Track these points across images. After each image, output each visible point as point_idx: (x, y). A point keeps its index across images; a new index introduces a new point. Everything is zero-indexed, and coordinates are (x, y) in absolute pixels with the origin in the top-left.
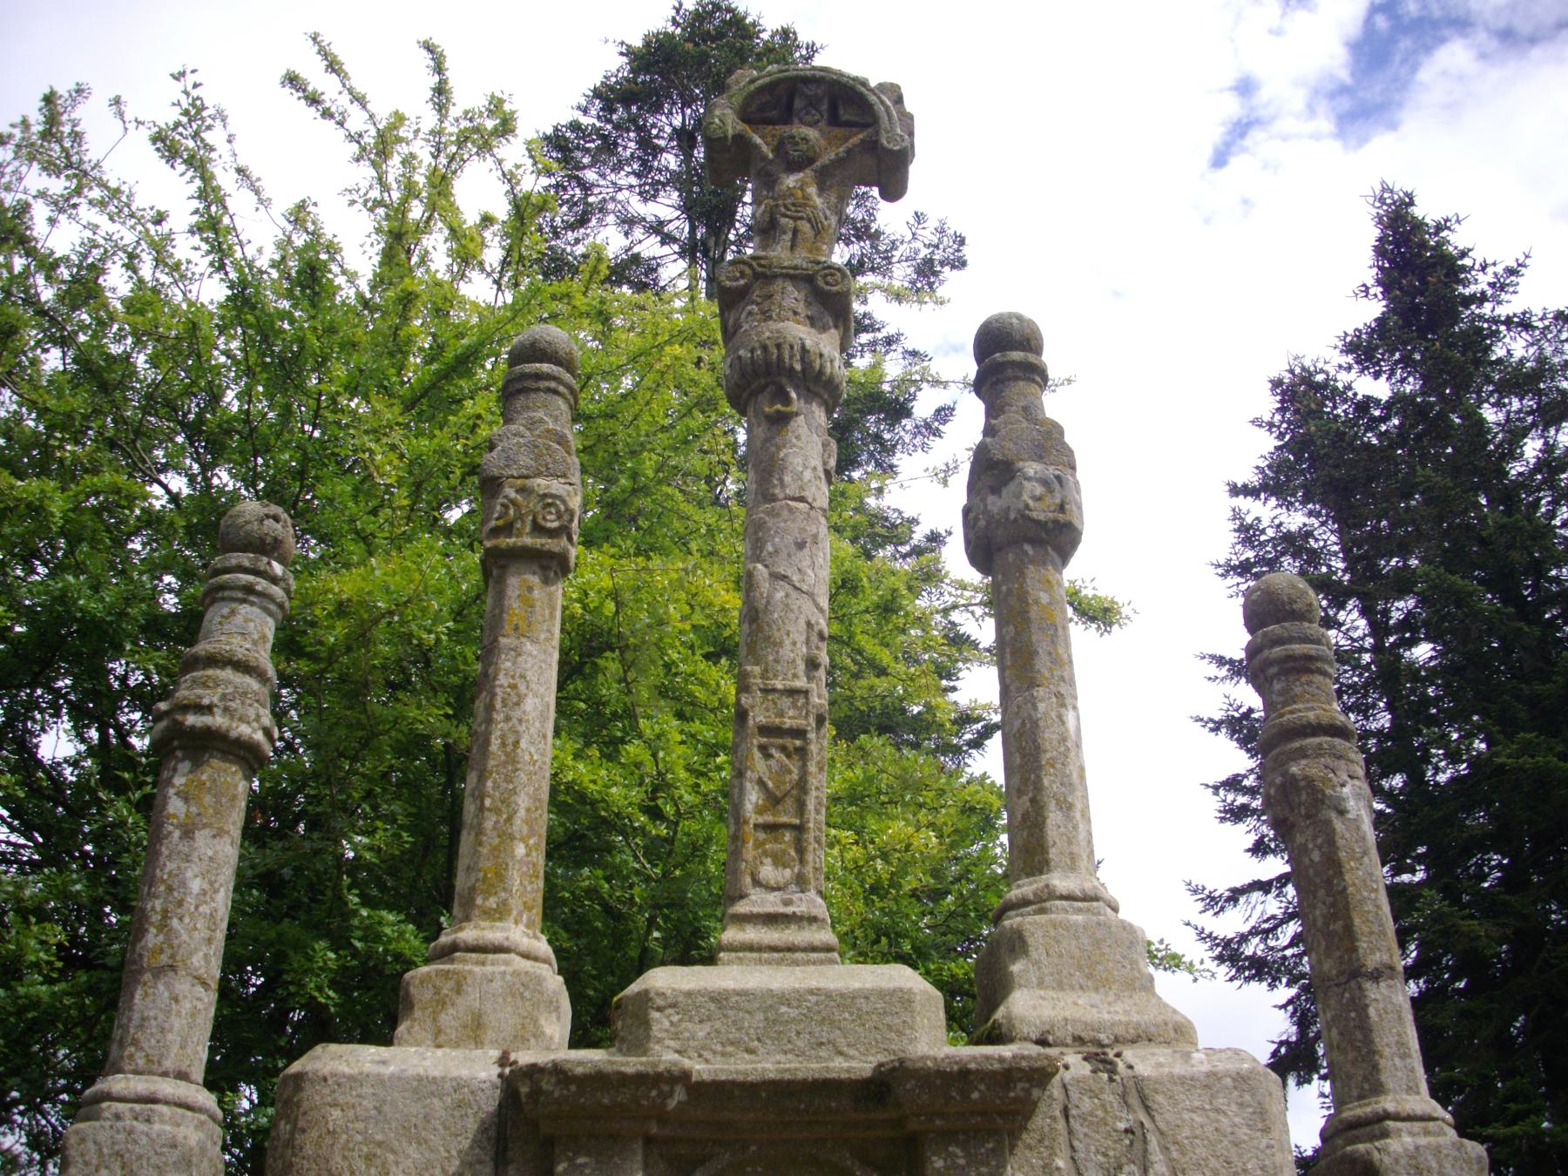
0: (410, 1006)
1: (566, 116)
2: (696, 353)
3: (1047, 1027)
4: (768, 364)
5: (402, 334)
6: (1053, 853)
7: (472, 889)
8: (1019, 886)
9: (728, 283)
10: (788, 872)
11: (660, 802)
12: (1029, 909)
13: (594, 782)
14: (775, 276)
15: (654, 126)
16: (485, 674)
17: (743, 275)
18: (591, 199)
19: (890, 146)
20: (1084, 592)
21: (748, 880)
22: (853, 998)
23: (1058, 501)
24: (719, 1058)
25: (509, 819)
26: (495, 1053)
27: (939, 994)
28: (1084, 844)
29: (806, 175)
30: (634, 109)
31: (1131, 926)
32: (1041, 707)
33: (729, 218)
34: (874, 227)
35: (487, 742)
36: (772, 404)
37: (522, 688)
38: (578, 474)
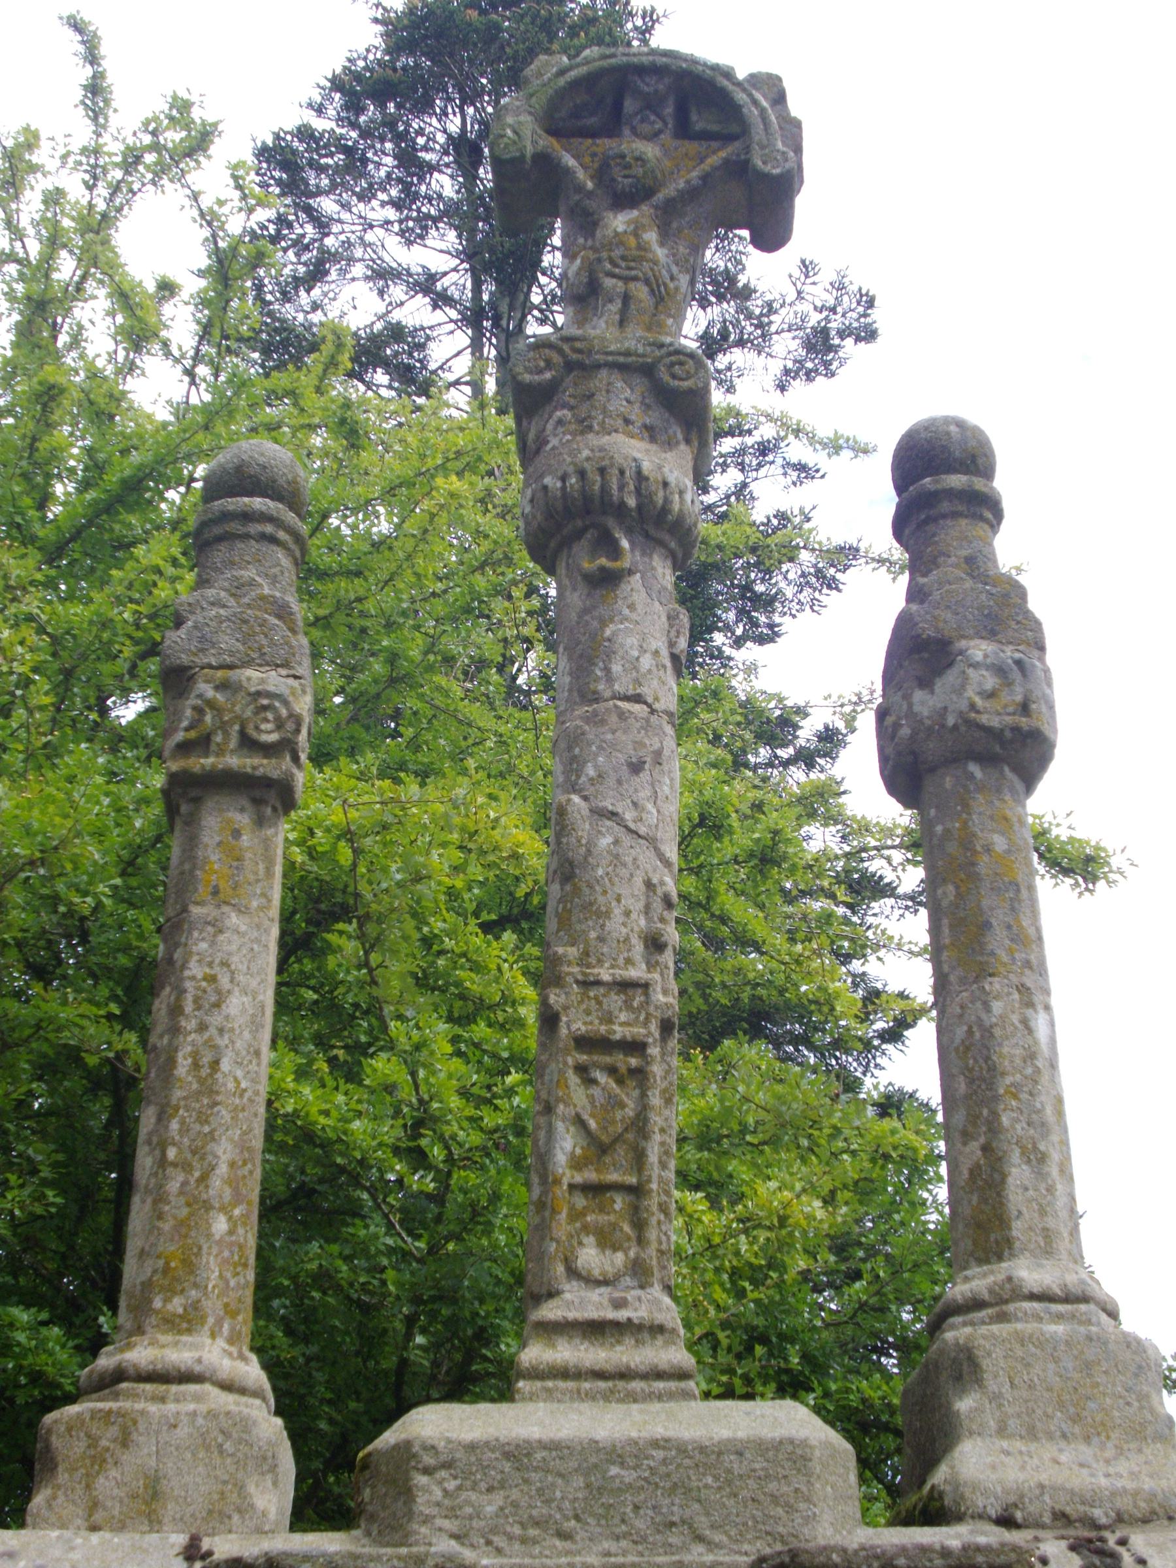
0: (51, 1466)
1: (291, 117)
2: (482, 484)
3: (1012, 1499)
4: (587, 498)
5: (40, 445)
6: (1017, 1229)
7: (147, 1285)
8: (967, 1279)
9: (527, 378)
10: (619, 1258)
11: (423, 1142)
12: (983, 1314)
13: (326, 1113)
14: (598, 366)
15: (421, 132)
16: (170, 961)
17: (549, 364)
18: (329, 241)
19: (767, 169)
20: (1055, 832)
21: (560, 1269)
22: (720, 1453)
23: (1019, 698)
24: (517, 1546)
25: (204, 1178)
26: (180, 1540)
27: (848, 1447)
28: (1063, 1214)
29: (641, 213)
30: (391, 107)
31: (1138, 1341)
32: (997, 1007)
33: (530, 267)
34: (742, 280)
35: (171, 1062)
36: (593, 558)
37: (224, 981)
38: (307, 662)
